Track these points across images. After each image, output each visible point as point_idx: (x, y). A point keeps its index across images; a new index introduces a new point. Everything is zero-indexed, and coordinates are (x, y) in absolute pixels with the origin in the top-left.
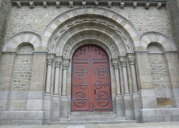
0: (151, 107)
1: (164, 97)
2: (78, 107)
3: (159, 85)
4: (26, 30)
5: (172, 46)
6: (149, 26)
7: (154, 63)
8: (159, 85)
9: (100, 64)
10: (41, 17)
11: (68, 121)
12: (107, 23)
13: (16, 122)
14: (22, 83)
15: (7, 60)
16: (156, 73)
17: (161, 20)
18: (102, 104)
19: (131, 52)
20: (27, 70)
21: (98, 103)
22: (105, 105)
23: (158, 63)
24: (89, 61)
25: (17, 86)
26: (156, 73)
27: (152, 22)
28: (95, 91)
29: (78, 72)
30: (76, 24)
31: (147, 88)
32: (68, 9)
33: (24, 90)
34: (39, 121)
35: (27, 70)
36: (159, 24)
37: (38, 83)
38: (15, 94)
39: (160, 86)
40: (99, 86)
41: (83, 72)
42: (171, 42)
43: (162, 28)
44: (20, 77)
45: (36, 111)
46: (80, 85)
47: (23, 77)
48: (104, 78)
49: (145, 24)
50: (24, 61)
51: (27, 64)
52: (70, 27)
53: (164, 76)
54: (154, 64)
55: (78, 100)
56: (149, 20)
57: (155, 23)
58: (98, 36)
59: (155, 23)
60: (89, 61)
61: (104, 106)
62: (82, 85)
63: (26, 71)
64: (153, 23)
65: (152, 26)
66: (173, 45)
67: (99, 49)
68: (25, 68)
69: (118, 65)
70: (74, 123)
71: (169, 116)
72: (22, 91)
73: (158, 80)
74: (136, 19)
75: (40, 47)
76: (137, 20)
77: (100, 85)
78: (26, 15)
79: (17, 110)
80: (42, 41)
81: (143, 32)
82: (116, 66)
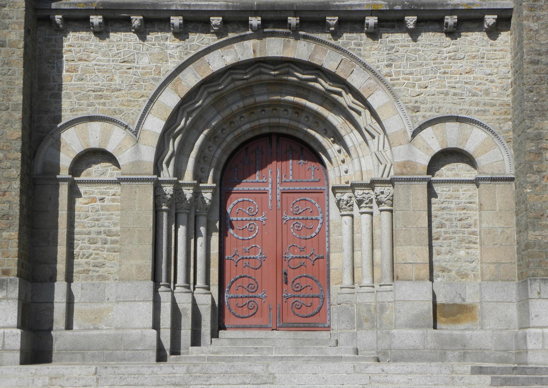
0: (417, 327)
1: (458, 301)
2: (239, 317)
3: (450, 271)
4: (90, 112)
5: (503, 160)
6: (447, 94)
7: (443, 209)
8: (450, 271)
9: (303, 196)
10: (129, 65)
11: (213, 353)
12: (322, 85)
13: (93, 356)
14: (95, 259)
15: (50, 199)
16: (448, 235)
17: (489, 71)
18: (306, 311)
19: (382, 176)
20: (106, 227)
21: (292, 309)
22: (311, 313)
23: (457, 209)
24: (269, 188)
25: (83, 269)
26: (448, 235)
27: (457, 83)
28: (285, 274)
29: (314, 217)
30: (232, 85)
31: (414, 278)
32: (210, 39)
33: (102, 278)
34: (148, 354)
35: (106, 227)
36: (480, 87)
37: (140, 262)
38: (80, 290)
39: (453, 273)
40: (298, 262)
41: (253, 218)
42: (502, 147)
43: (487, 99)
44: (87, 244)
45: (139, 331)
46: (243, 258)
47: (96, 245)
48: (312, 237)
49: (434, 89)
50: (94, 200)
51: (102, 210)
52: (213, 96)
53: (467, 245)
54: (445, 212)
55: (237, 297)
56: (449, 75)
57: (466, 83)
58: (297, 113)
59: (466, 83)
60: (269, 188)
61: (309, 317)
62: (250, 258)
63: (102, 229)
64: (459, 85)
65: (455, 94)
66: (506, 157)
67: (302, 149)
68: (98, 220)
69: (352, 205)
70: (230, 357)
71: (459, 350)
72: (96, 282)
73: (448, 257)
74: (408, 71)
75: (137, 163)
76: (411, 74)
77: (300, 258)
78: (85, 57)
79: (315, 357)
80: (139, 144)
81: (424, 117)
82: (344, 206)
